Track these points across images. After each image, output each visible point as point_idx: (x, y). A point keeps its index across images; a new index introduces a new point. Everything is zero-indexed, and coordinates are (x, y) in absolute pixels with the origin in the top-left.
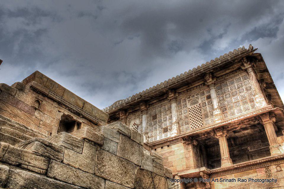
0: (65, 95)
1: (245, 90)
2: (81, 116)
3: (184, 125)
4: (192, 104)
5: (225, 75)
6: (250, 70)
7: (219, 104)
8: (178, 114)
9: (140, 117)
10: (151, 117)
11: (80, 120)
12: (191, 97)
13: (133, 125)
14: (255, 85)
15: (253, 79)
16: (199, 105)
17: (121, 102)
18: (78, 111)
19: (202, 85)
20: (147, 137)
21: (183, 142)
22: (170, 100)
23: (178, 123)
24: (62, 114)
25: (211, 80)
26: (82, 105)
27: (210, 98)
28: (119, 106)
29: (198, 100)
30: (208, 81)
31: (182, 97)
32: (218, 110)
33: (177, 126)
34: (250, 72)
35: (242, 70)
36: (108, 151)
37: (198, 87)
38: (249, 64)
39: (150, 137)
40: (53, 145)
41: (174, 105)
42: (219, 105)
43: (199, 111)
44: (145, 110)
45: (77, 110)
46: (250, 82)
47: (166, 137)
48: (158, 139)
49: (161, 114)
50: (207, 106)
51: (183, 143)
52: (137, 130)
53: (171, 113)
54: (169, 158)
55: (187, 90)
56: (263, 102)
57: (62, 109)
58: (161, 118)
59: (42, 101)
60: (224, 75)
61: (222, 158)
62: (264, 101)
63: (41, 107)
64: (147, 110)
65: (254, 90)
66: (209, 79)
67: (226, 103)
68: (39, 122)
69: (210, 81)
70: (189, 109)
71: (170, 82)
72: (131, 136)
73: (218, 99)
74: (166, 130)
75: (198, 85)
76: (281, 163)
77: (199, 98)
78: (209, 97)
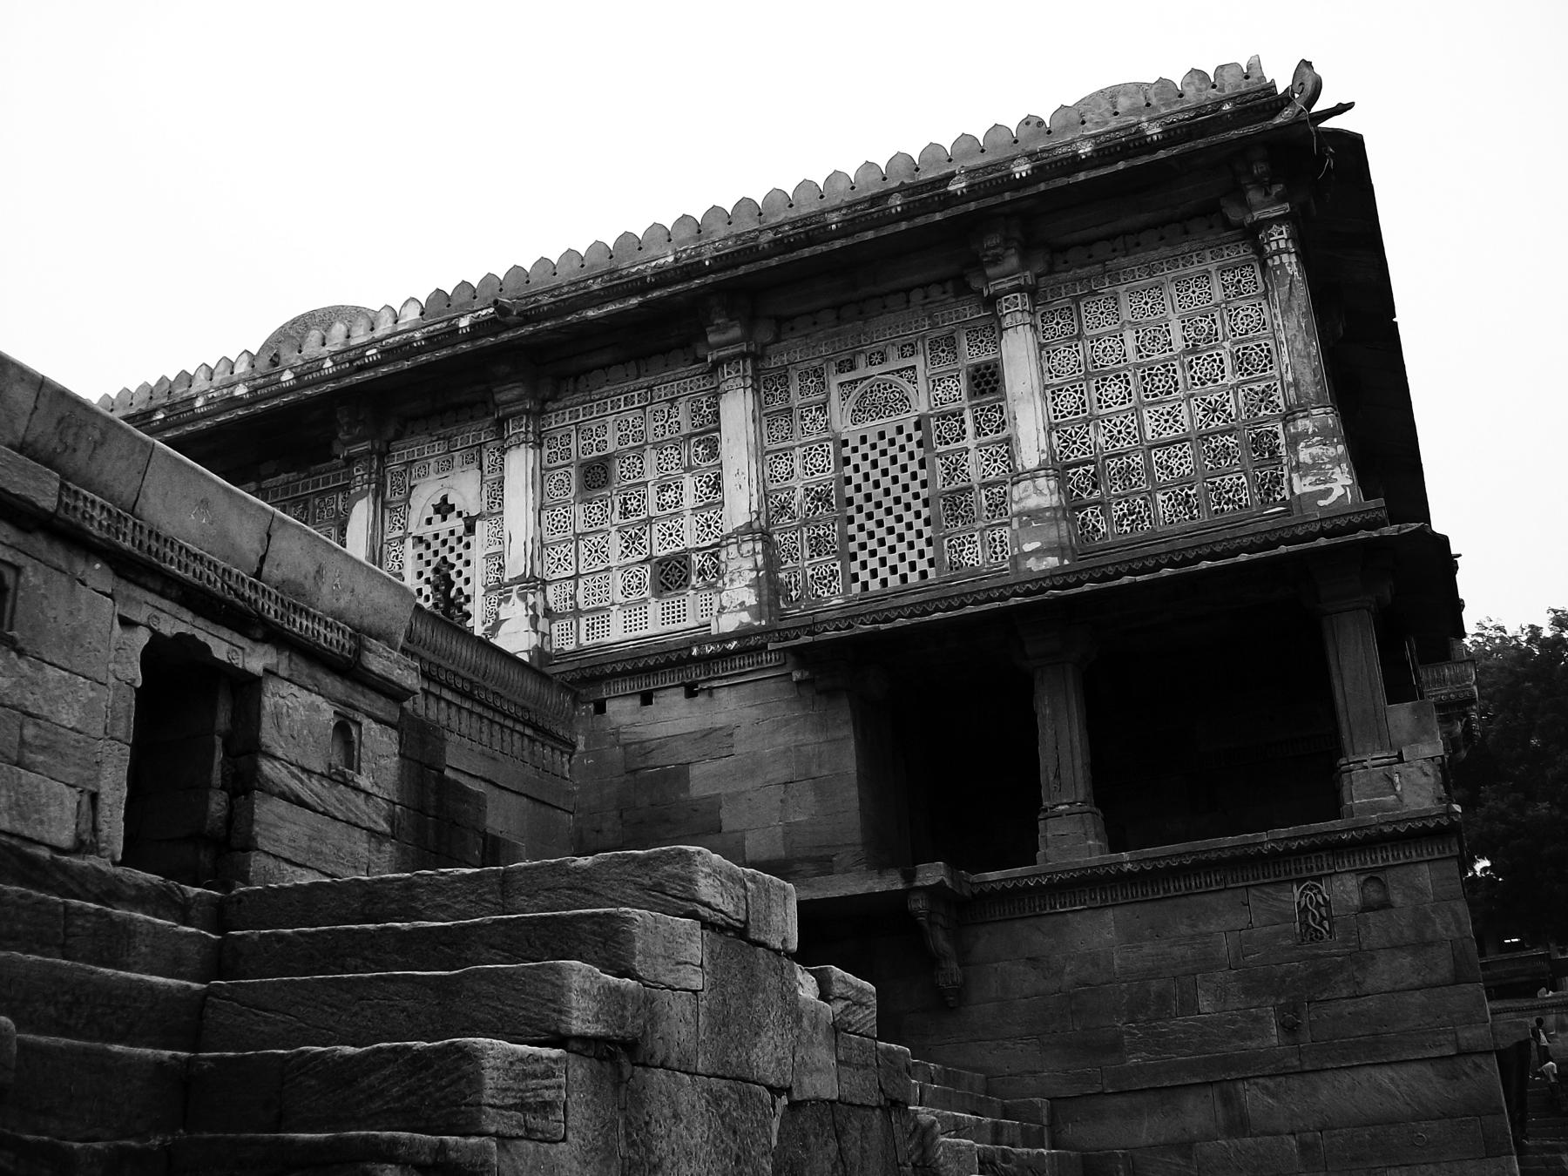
0: (150, 492)
1: (1234, 372)
2: (259, 634)
3: (807, 554)
4: (859, 414)
5: (1110, 238)
6: (1279, 238)
7: (1055, 441)
8: (767, 471)
9: (486, 463)
10: (572, 471)
11: (256, 660)
12: (861, 361)
13: (430, 512)
14: (1299, 345)
15: (1295, 304)
16: (918, 426)
17: (339, 330)
18: (242, 597)
19: (949, 286)
20: (540, 612)
21: (796, 675)
22: (717, 364)
23: (766, 537)
24: (142, 637)
25: (1013, 262)
26: (257, 546)
27: (993, 390)
28: (328, 363)
29: (912, 398)
30: (990, 272)
31: (790, 354)
32: (1041, 482)
33: (760, 558)
34: (1279, 252)
35: (1228, 225)
36: (662, 1066)
37: (916, 296)
38: (1281, 199)
39: (562, 616)
40: (453, 1155)
41: (737, 410)
42: (1050, 445)
43: (913, 466)
44: (527, 412)
45: (231, 597)
46: (1266, 316)
47: (672, 627)
48: (617, 631)
49: (640, 458)
50: (970, 441)
51: (798, 683)
52: (459, 549)
53: (714, 453)
54: (695, 771)
55: (837, 307)
56: (1337, 470)
57: (139, 603)
58: (645, 484)
59: (18, 570)
60: (1100, 239)
61: (1046, 804)
62: (1344, 466)
63: (19, 616)
64: (543, 412)
65: (1289, 378)
66: (996, 260)
67: (1101, 440)
68: (16, 732)
69: (1005, 274)
70: (845, 443)
71: (722, 234)
72: (746, 922)
73: (1051, 405)
74: (671, 575)
75: (921, 286)
76: (1392, 862)
77: (921, 379)
78: (987, 380)
